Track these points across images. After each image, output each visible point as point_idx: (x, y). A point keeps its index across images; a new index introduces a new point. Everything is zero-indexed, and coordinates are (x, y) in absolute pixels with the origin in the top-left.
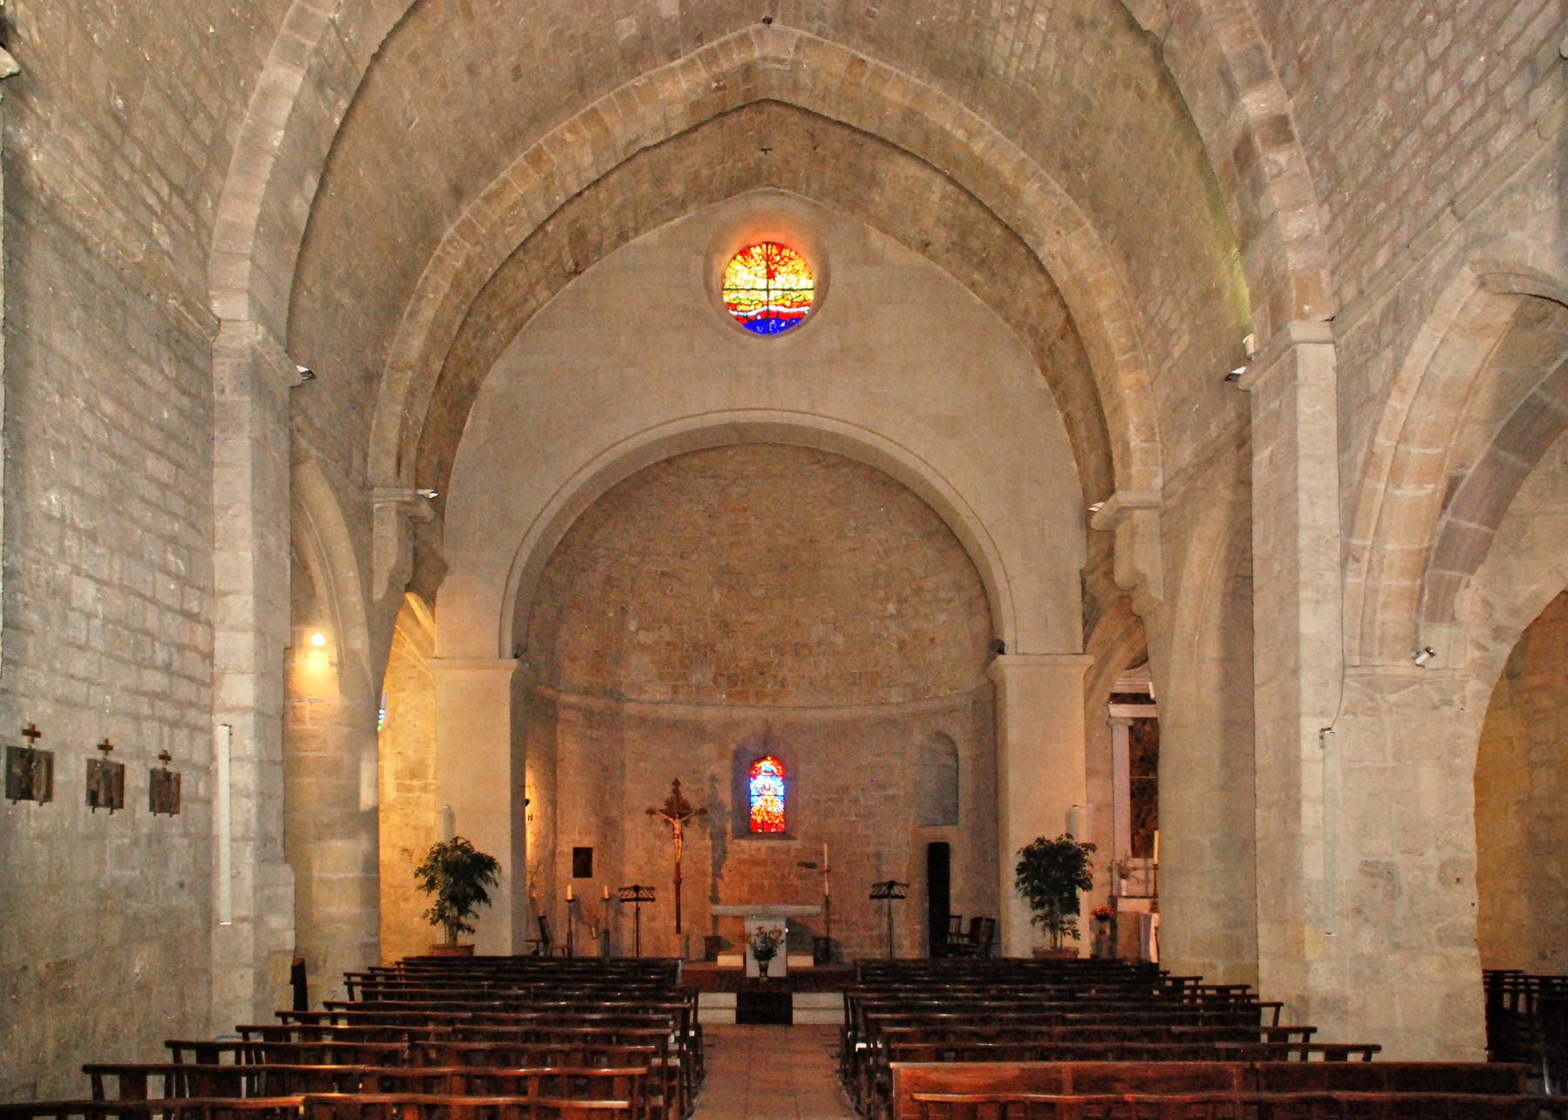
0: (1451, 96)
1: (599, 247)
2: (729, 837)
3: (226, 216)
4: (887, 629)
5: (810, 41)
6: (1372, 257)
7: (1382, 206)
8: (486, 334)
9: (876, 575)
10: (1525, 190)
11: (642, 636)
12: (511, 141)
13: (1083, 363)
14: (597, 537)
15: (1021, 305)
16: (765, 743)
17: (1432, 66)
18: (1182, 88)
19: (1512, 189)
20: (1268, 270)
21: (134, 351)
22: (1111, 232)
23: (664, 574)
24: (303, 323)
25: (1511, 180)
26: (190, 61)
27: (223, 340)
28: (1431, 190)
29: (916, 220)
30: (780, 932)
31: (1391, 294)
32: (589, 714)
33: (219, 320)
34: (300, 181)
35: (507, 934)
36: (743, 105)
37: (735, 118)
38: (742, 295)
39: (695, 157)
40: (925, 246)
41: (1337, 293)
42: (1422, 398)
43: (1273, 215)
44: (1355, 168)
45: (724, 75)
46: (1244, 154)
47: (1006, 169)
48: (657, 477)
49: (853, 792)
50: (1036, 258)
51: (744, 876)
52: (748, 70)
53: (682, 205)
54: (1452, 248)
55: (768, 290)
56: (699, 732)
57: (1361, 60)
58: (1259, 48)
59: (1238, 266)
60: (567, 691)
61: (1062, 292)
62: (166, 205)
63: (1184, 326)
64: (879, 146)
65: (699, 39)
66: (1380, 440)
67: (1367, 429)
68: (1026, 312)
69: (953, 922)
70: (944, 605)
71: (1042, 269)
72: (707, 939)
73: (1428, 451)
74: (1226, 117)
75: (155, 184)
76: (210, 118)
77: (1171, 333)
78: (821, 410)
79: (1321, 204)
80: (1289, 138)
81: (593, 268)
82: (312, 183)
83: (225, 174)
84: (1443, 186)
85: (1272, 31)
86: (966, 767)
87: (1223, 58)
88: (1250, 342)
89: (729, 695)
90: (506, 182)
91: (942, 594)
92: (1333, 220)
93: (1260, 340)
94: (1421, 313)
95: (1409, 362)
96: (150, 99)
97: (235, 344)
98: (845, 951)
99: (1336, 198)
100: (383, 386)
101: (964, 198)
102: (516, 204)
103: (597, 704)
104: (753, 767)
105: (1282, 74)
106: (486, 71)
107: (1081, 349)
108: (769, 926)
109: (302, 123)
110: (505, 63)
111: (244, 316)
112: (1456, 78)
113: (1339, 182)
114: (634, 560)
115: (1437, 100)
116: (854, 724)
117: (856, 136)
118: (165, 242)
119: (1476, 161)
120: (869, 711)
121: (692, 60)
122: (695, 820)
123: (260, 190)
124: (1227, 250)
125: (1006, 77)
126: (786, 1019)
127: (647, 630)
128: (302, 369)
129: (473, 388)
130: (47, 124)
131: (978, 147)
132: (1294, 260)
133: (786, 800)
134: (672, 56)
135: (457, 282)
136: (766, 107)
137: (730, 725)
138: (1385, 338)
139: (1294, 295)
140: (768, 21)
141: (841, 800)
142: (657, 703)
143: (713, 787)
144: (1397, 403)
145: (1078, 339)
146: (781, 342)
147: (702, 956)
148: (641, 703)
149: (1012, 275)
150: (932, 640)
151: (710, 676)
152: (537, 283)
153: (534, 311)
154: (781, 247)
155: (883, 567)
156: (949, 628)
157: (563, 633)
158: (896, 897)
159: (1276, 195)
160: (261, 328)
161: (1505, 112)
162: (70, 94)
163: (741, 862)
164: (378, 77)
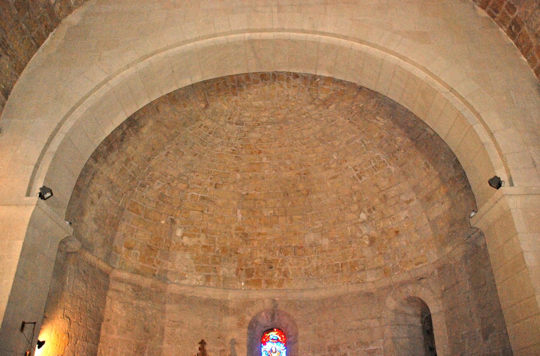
4: (361, 231)
11: (186, 240)
14: (153, 163)
16: (273, 317)
23: (203, 198)
56: (223, 307)
60: (120, 269)
78: (320, 29)
89: (247, 283)
103: (147, 282)
104: (263, 336)
114: (182, 186)
116: (339, 299)
120: (352, 289)
127: (190, 236)
142: (193, 286)
143: (233, 349)
148: (182, 285)
150: (397, 232)
151: (233, 270)
155: (356, 187)
157: (123, 228)
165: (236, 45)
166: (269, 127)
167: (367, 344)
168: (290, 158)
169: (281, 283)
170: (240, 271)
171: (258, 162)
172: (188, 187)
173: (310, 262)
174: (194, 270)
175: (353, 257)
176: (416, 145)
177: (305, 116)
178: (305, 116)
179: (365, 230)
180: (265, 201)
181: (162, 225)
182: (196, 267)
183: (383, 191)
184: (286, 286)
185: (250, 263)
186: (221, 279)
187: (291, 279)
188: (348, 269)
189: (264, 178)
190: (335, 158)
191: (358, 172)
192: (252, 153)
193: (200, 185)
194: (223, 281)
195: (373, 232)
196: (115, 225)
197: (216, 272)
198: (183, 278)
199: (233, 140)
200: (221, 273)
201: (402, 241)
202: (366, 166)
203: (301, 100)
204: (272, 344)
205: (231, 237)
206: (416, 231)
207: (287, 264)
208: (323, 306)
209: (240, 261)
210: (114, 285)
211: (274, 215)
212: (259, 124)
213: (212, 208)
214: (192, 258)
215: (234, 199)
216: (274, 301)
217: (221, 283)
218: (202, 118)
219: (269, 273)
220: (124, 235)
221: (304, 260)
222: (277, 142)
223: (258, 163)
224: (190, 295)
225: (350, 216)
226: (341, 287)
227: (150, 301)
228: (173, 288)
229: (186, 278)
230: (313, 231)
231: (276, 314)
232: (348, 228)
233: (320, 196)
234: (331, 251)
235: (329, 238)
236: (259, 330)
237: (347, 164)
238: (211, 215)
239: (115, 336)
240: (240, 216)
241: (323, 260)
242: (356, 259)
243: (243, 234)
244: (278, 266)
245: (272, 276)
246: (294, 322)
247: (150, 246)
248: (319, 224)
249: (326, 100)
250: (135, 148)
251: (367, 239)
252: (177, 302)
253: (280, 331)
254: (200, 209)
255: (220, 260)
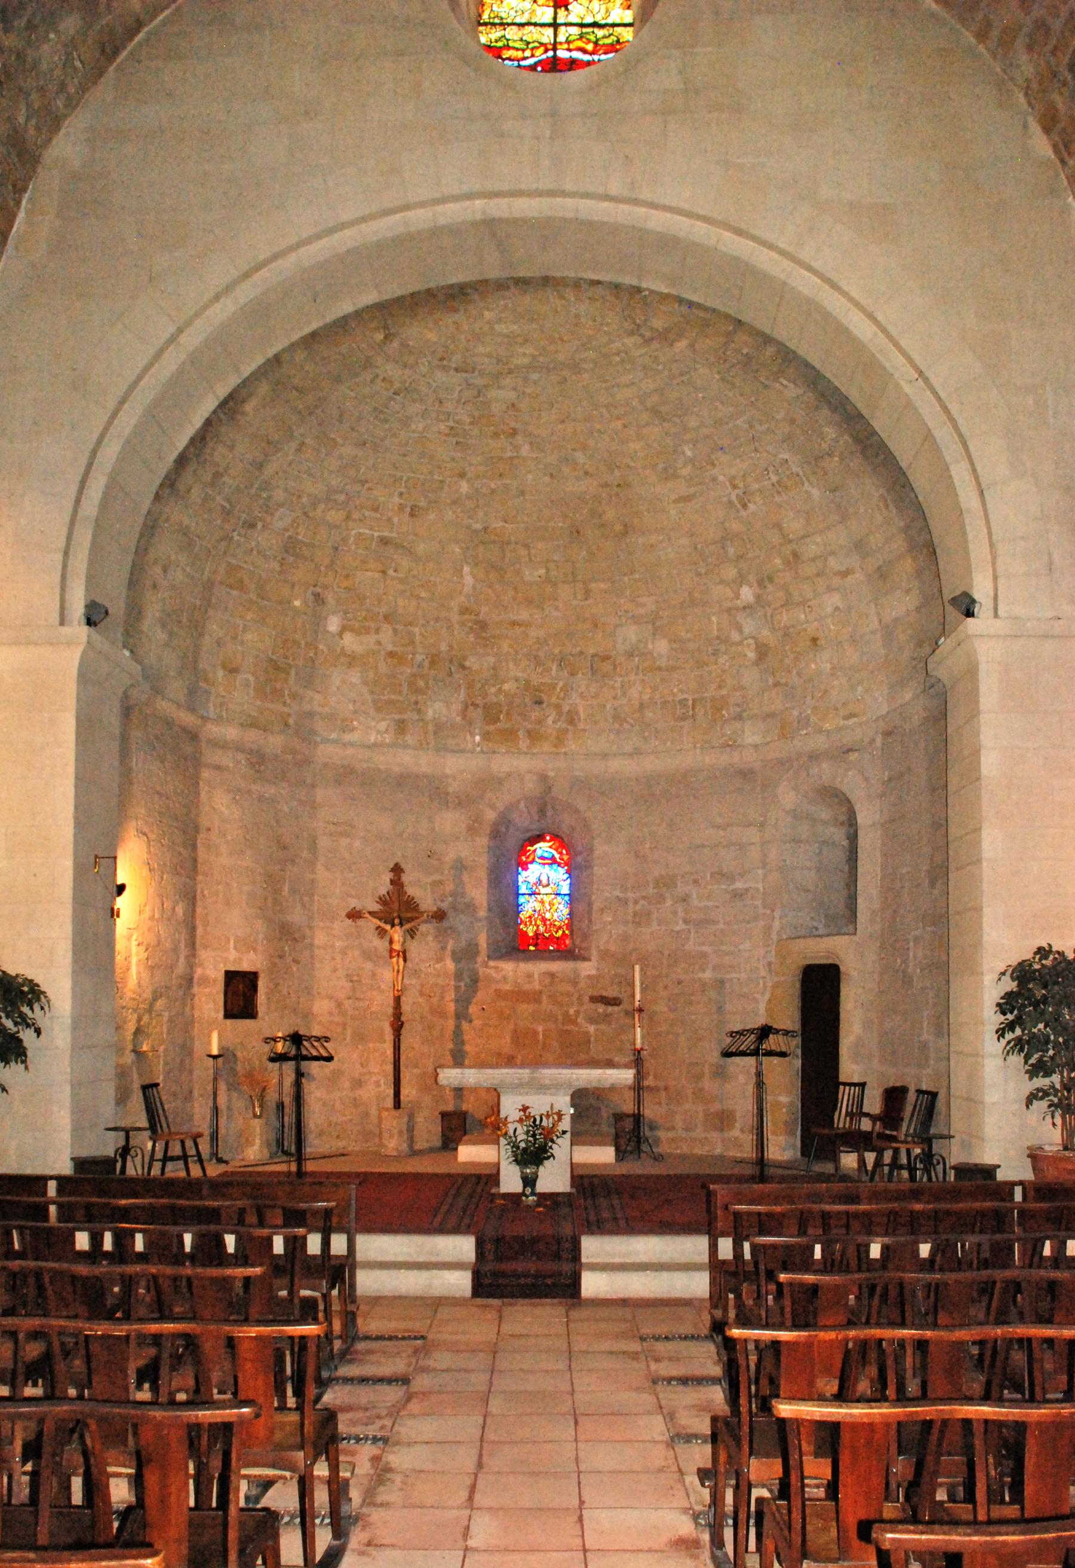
2: (482, 957)
4: (740, 629)
9: (726, 538)
11: (349, 641)
14: (269, 470)
16: (542, 811)
23: (384, 541)
30: (560, 1115)
32: (258, 760)
35: (63, 1118)
38: (512, 33)
48: (368, 364)
49: (681, 889)
51: (501, 1015)
55: (555, 25)
56: (436, 792)
60: (219, 720)
69: (845, 1096)
70: (836, 581)
72: (444, 1115)
78: (646, 195)
86: (869, 841)
89: (486, 736)
91: (833, 563)
98: (662, 1134)
104: (523, 851)
108: (539, 1105)
114: (335, 516)
120: (709, 759)
122: (426, 928)
126: (568, 1288)
127: (357, 632)
133: (573, 898)
137: (488, 782)
141: (662, 898)
147: (437, 1142)
150: (814, 640)
151: (457, 707)
155: (735, 526)
156: (851, 615)
157: (214, 628)
158: (770, 1053)
163: (500, 995)
165: (455, 231)
166: (535, 376)
167: (731, 878)
168: (584, 448)
169: (560, 739)
170: (471, 708)
171: (509, 454)
172: (348, 517)
173: (624, 694)
174: (372, 712)
175: (720, 687)
176: (863, 451)
177: (618, 359)
178: (618, 359)
179: (749, 626)
180: (526, 546)
181: (297, 612)
182: (374, 702)
183: (790, 541)
184: (571, 746)
185: (493, 690)
186: (431, 728)
187: (584, 730)
188: (706, 714)
189: (523, 493)
190: (689, 453)
191: (739, 492)
192: (496, 435)
193: (376, 509)
194: (435, 733)
195: (765, 633)
196: (198, 628)
197: (419, 711)
198: (347, 729)
199: (449, 406)
200: (430, 713)
201: (822, 663)
202: (757, 480)
203: (608, 324)
204: (540, 867)
205: (450, 628)
206: (853, 641)
207: (574, 695)
208: (652, 792)
209: (470, 685)
210: (213, 756)
211: (548, 580)
212: (510, 372)
213: (405, 563)
214: (366, 683)
215: (457, 542)
216: (544, 778)
217: (431, 736)
218: (379, 360)
219: (535, 715)
220: (219, 643)
221: (613, 687)
222: (554, 410)
223: (511, 458)
224: (365, 766)
225: (718, 592)
226: (686, 754)
227: (284, 785)
228: (326, 753)
229: (353, 729)
230: (636, 620)
231: (549, 807)
232: (714, 618)
233: (653, 539)
234: (674, 668)
235: (670, 641)
236: (512, 842)
237: (715, 471)
238: (403, 581)
239: (224, 860)
240: (469, 580)
241: (654, 689)
242: (724, 692)
243: (476, 622)
244: (554, 700)
245: (540, 722)
246: (586, 825)
247: (275, 662)
248: (649, 604)
249: (667, 330)
250: (233, 453)
251: (753, 646)
252: (338, 783)
253: (559, 840)
254: (380, 567)
255: (427, 684)
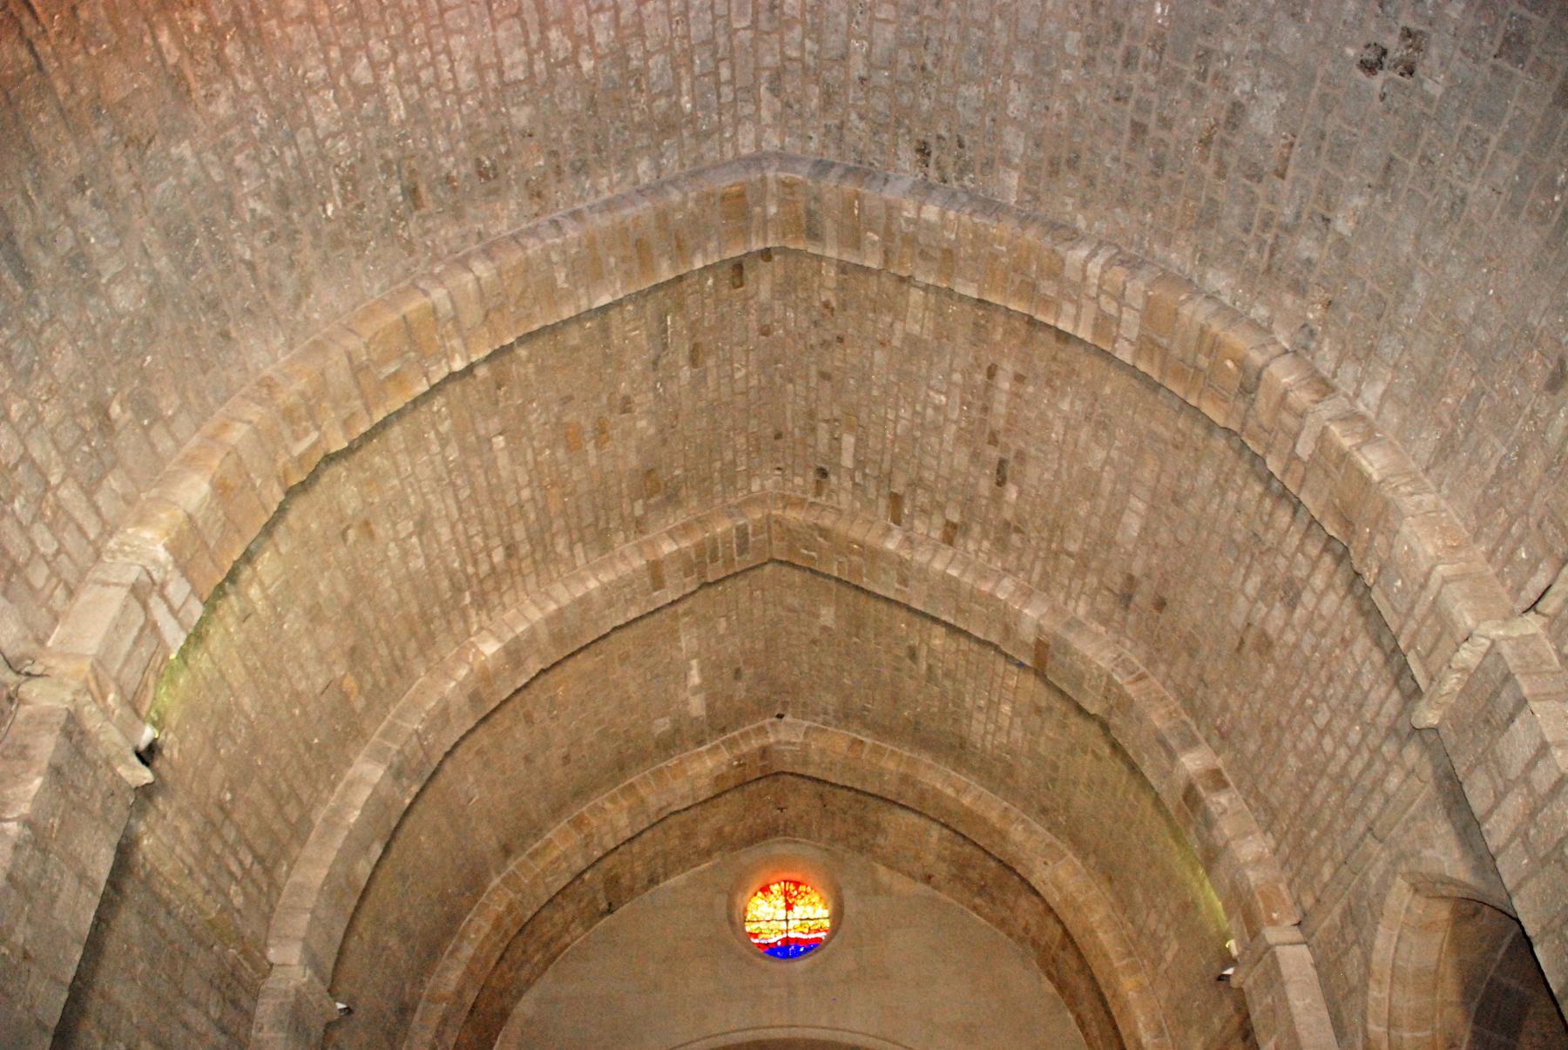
0: (1343, 753)
1: (631, 889)
3: (296, 878)
5: (817, 729)
6: (1318, 873)
7: (1314, 833)
8: (521, 966)
10: (1424, 819)
12: (556, 812)
13: (1084, 967)
15: (1021, 922)
17: (1321, 733)
18: (1130, 752)
19: (1413, 819)
20: (1234, 887)
21: (186, 996)
22: (1092, 860)
24: (351, 963)
25: (1412, 809)
26: (294, 763)
27: (275, 982)
28: (1351, 818)
29: (917, 858)
31: (1344, 901)
33: (272, 965)
34: (367, 848)
36: (762, 776)
37: (753, 787)
39: (718, 817)
40: (928, 879)
41: (1298, 902)
42: (1398, 987)
43: (1227, 843)
44: (1284, 805)
45: (744, 756)
46: (1190, 796)
47: (994, 816)
50: (1029, 885)
52: (764, 752)
53: (708, 853)
54: (1380, 864)
57: (1266, 730)
58: (1184, 723)
59: (1207, 883)
61: (1057, 911)
62: (247, 872)
63: (1172, 934)
64: (881, 803)
65: (723, 730)
66: (1372, 1027)
67: (1357, 1020)
68: (1026, 929)
71: (1037, 893)
73: (1419, 1034)
74: (1169, 773)
75: (241, 856)
76: (300, 802)
77: (1161, 941)
79: (1265, 832)
80: (1226, 785)
81: (626, 907)
82: (377, 850)
83: (303, 844)
84: (1359, 818)
85: (1192, 711)
87: (1156, 731)
88: (1231, 944)
90: (550, 841)
92: (1279, 844)
93: (1240, 942)
94: (1373, 915)
95: (1375, 957)
96: (255, 791)
97: (283, 986)
99: (1276, 827)
100: (417, 1017)
101: (961, 840)
102: (558, 858)
105: (1207, 740)
106: (540, 761)
107: (1080, 956)
109: (378, 803)
110: (556, 753)
111: (295, 961)
112: (1342, 740)
113: (1275, 816)
115: (1333, 755)
117: (860, 797)
118: (238, 901)
119: (1378, 798)
121: (717, 747)
123: (331, 856)
124: (1194, 871)
125: (984, 751)
128: (340, 1006)
129: (504, 1015)
130: (164, 817)
131: (966, 800)
132: (1253, 877)
134: (701, 743)
135: (497, 925)
136: (782, 778)
138: (1350, 938)
139: (1261, 905)
140: (780, 716)
144: (1377, 993)
145: (1077, 949)
146: (801, 964)
149: (1010, 897)
152: (573, 921)
153: (567, 945)
154: (797, 884)
159: (1226, 828)
160: (308, 972)
161: (1388, 764)
162: (189, 792)
164: (448, 766)
